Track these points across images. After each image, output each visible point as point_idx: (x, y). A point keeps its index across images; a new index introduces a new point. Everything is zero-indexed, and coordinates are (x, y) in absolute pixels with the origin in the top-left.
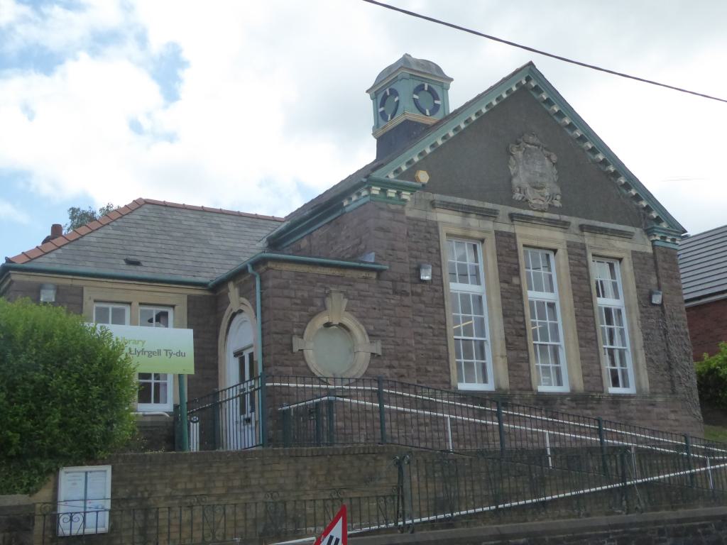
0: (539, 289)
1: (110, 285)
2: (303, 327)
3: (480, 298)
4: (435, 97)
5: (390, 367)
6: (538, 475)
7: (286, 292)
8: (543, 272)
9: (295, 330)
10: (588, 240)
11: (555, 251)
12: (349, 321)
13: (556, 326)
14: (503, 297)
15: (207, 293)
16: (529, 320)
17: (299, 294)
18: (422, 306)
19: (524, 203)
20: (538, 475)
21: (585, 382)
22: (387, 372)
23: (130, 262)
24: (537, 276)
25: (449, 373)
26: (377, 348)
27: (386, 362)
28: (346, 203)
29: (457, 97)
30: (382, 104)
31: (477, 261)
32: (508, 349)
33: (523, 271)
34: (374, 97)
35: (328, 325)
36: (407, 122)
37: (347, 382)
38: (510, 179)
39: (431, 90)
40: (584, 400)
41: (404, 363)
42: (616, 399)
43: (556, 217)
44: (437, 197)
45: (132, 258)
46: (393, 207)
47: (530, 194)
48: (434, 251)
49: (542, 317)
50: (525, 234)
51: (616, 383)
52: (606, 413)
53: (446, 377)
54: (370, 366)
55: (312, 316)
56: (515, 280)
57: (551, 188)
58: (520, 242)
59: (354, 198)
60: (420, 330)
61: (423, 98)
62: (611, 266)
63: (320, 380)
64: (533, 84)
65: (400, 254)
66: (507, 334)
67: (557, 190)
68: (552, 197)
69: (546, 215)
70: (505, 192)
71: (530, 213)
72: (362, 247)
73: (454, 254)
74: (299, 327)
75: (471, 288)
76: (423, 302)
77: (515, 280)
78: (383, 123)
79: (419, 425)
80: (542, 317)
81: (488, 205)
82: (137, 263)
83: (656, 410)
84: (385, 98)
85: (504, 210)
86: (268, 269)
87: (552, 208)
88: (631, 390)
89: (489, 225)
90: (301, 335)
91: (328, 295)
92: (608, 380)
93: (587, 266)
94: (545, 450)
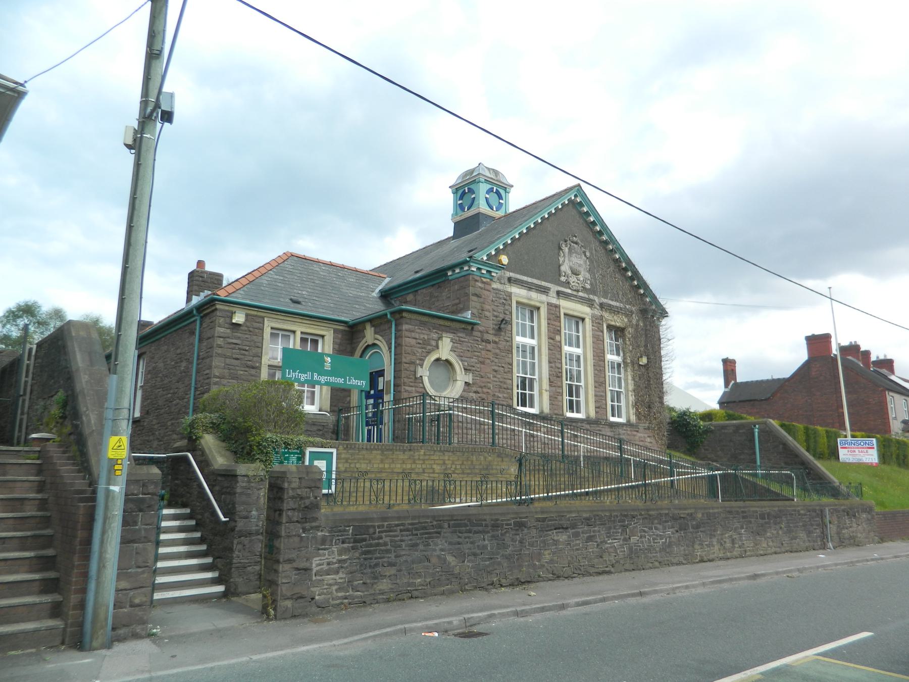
0: (524, 335)
1: (255, 313)
4: (500, 197)
5: (476, 392)
6: (324, 460)
7: (413, 335)
8: (528, 323)
9: (418, 362)
10: (606, 315)
13: (534, 364)
14: (549, 349)
15: (347, 329)
17: (422, 336)
18: (498, 351)
19: (567, 284)
20: (324, 460)
21: (596, 412)
22: (474, 396)
24: (524, 326)
26: (469, 378)
27: (474, 389)
28: (450, 273)
29: (516, 201)
30: (461, 198)
32: (550, 385)
33: (563, 331)
34: (455, 192)
35: (438, 360)
36: (478, 214)
37: (451, 400)
38: (559, 266)
39: (498, 193)
40: (595, 424)
41: (485, 390)
44: (512, 275)
46: (484, 280)
47: (573, 279)
50: (567, 306)
51: (571, 409)
53: (510, 402)
54: (464, 391)
55: (429, 353)
57: (584, 275)
58: (562, 312)
59: (457, 271)
60: (496, 368)
61: (493, 198)
62: (532, 313)
64: (579, 200)
65: (487, 314)
66: (550, 375)
67: (588, 276)
69: (581, 294)
70: (555, 275)
71: (569, 291)
74: (421, 360)
75: (528, 341)
76: (499, 349)
77: (558, 338)
78: (460, 212)
80: (524, 356)
81: (544, 284)
83: (639, 435)
84: (464, 193)
85: (554, 288)
86: (402, 317)
87: (584, 289)
88: (622, 420)
89: (543, 297)
90: (422, 366)
91: (440, 338)
92: (566, 405)
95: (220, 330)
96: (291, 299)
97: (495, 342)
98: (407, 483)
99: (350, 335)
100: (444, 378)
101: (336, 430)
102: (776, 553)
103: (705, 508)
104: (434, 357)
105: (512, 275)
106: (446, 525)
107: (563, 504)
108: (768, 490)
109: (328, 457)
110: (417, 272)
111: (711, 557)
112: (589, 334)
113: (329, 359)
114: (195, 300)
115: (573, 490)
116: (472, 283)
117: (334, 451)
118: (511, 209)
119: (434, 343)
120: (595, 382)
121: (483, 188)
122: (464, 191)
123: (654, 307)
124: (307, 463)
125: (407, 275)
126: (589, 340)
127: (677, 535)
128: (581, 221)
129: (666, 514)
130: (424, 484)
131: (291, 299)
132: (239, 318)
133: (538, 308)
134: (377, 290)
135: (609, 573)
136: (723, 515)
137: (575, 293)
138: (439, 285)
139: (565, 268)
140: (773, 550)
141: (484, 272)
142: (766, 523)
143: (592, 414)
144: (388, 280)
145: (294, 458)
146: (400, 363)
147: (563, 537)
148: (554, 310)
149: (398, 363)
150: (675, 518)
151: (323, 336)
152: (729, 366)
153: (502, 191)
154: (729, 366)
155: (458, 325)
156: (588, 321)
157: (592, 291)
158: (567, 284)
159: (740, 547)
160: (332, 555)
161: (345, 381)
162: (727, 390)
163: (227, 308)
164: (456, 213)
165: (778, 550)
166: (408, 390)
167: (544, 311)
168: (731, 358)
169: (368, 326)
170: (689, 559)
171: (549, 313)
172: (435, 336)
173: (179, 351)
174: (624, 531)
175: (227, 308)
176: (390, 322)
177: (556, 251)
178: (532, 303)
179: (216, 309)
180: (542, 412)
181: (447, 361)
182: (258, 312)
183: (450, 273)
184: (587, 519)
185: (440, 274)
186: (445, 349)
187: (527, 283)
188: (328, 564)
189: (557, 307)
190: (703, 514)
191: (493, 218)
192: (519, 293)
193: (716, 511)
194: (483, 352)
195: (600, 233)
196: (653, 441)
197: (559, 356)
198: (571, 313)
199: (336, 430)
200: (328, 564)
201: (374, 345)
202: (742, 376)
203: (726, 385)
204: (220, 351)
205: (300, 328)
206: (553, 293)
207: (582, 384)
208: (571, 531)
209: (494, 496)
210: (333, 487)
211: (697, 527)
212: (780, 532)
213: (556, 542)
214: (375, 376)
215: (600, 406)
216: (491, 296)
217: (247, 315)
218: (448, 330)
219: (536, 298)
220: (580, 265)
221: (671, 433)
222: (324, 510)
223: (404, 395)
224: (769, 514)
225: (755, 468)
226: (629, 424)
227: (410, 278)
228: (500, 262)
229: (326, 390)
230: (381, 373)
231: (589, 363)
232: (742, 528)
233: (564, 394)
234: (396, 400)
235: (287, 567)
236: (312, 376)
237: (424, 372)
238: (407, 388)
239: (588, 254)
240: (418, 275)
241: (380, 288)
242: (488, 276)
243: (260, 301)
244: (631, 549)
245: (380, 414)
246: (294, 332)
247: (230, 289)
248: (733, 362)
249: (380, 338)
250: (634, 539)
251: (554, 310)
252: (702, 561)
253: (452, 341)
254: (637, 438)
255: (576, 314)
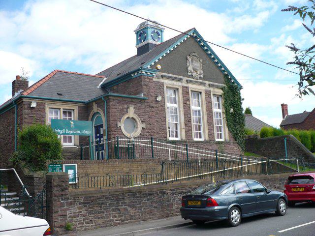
2: (120, 119)
3: (176, 108)
10: (211, 89)
11: (201, 93)
12: (135, 117)
13: (177, 116)
16: (192, 116)
19: (192, 76)
23: (59, 94)
25: (166, 134)
26: (144, 126)
28: (132, 75)
29: (167, 36)
31: (175, 96)
34: (137, 33)
35: (128, 118)
38: (187, 68)
39: (157, 33)
40: (210, 142)
41: (152, 131)
42: (219, 143)
43: (201, 81)
44: (163, 74)
45: (59, 93)
46: (149, 78)
47: (194, 74)
48: (162, 92)
49: (217, 117)
52: (215, 147)
55: (123, 115)
56: (188, 103)
57: (200, 71)
59: (136, 74)
63: (128, 138)
64: (195, 35)
67: (202, 72)
68: (200, 74)
69: (198, 80)
70: (185, 72)
71: (192, 79)
72: (138, 91)
73: (169, 94)
74: (119, 119)
77: (188, 103)
79: (157, 151)
80: (217, 117)
81: (180, 77)
82: (61, 95)
84: (141, 34)
85: (185, 79)
86: (109, 99)
87: (200, 78)
88: (223, 140)
89: (180, 84)
90: (120, 122)
91: (128, 108)
93: (211, 98)
94: (198, 160)
95: (25, 111)
96: (58, 94)
97: (156, 107)
98: (108, 177)
99: (86, 110)
100: (130, 129)
101: (81, 154)
105: (163, 74)
106: (127, 195)
107: (184, 182)
108: (285, 167)
109: (73, 168)
110: (118, 75)
112: (204, 99)
113: (73, 123)
114: (16, 94)
115: (189, 176)
116: (143, 79)
117: (76, 165)
118: (164, 40)
119: (125, 110)
120: (208, 123)
121: (150, 31)
122: (141, 33)
123: (236, 84)
124: (64, 171)
125: (114, 76)
126: (204, 102)
128: (197, 45)
130: (119, 177)
131: (58, 94)
132: (34, 105)
133: (178, 89)
134: (100, 85)
137: (195, 80)
138: (128, 81)
139: (190, 68)
141: (149, 74)
143: (207, 138)
144: (105, 79)
145: (58, 169)
146: (109, 121)
148: (186, 91)
149: (108, 121)
151: (73, 110)
152: (284, 107)
153: (159, 32)
154: (284, 107)
155: (137, 101)
156: (203, 93)
157: (204, 79)
158: (192, 76)
160: (75, 209)
161: (81, 132)
162: (284, 119)
163: (28, 100)
164: (138, 44)
166: (114, 133)
167: (180, 90)
168: (285, 103)
169: (94, 104)
171: (183, 91)
172: (126, 106)
173: (9, 121)
175: (28, 100)
176: (103, 101)
177: (185, 60)
178: (175, 87)
179: (23, 101)
180: (182, 139)
181: (133, 118)
182: (42, 102)
183: (132, 75)
185: (129, 75)
186: (131, 112)
187: (171, 77)
188: (74, 213)
189: (187, 88)
191: (156, 46)
192: (167, 82)
194: (151, 113)
197: (189, 112)
198: (193, 90)
199: (81, 154)
200: (74, 213)
201: (98, 113)
202: (291, 112)
203: (284, 117)
204: (26, 120)
205: (62, 107)
206: (184, 81)
207: (202, 124)
209: (153, 181)
210: (77, 181)
214: (98, 128)
215: (211, 134)
216: (153, 85)
217: (37, 103)
218: (132, 103)
219: (176, 84)
220: (197, 67)
221: (246, 143)
222: (70, 190)
223: (113, 136)
225: (286, 158)
226: (225, 142)
227: (117, 78)
228: (157, 68)
229: (77, 137)
230: (101, 126)
231: (204, 114)
233: (193, 130)
234: (109, 139)
235: (56, 214)
236: (66, 131)
237: (122, 125)
238: (113, 133)
239: (201, 61)
240: (119, 76)
241: (101, 83)
242: (151, 75)
243: (43, 96)
245: (103, 147)
246: (60, 109)
247: (32, 89)
248: (286, 106)
249: (100, 109)
251: (186, 91)
253: (134, 108)
254: (230, 148)
255: (196, 90)
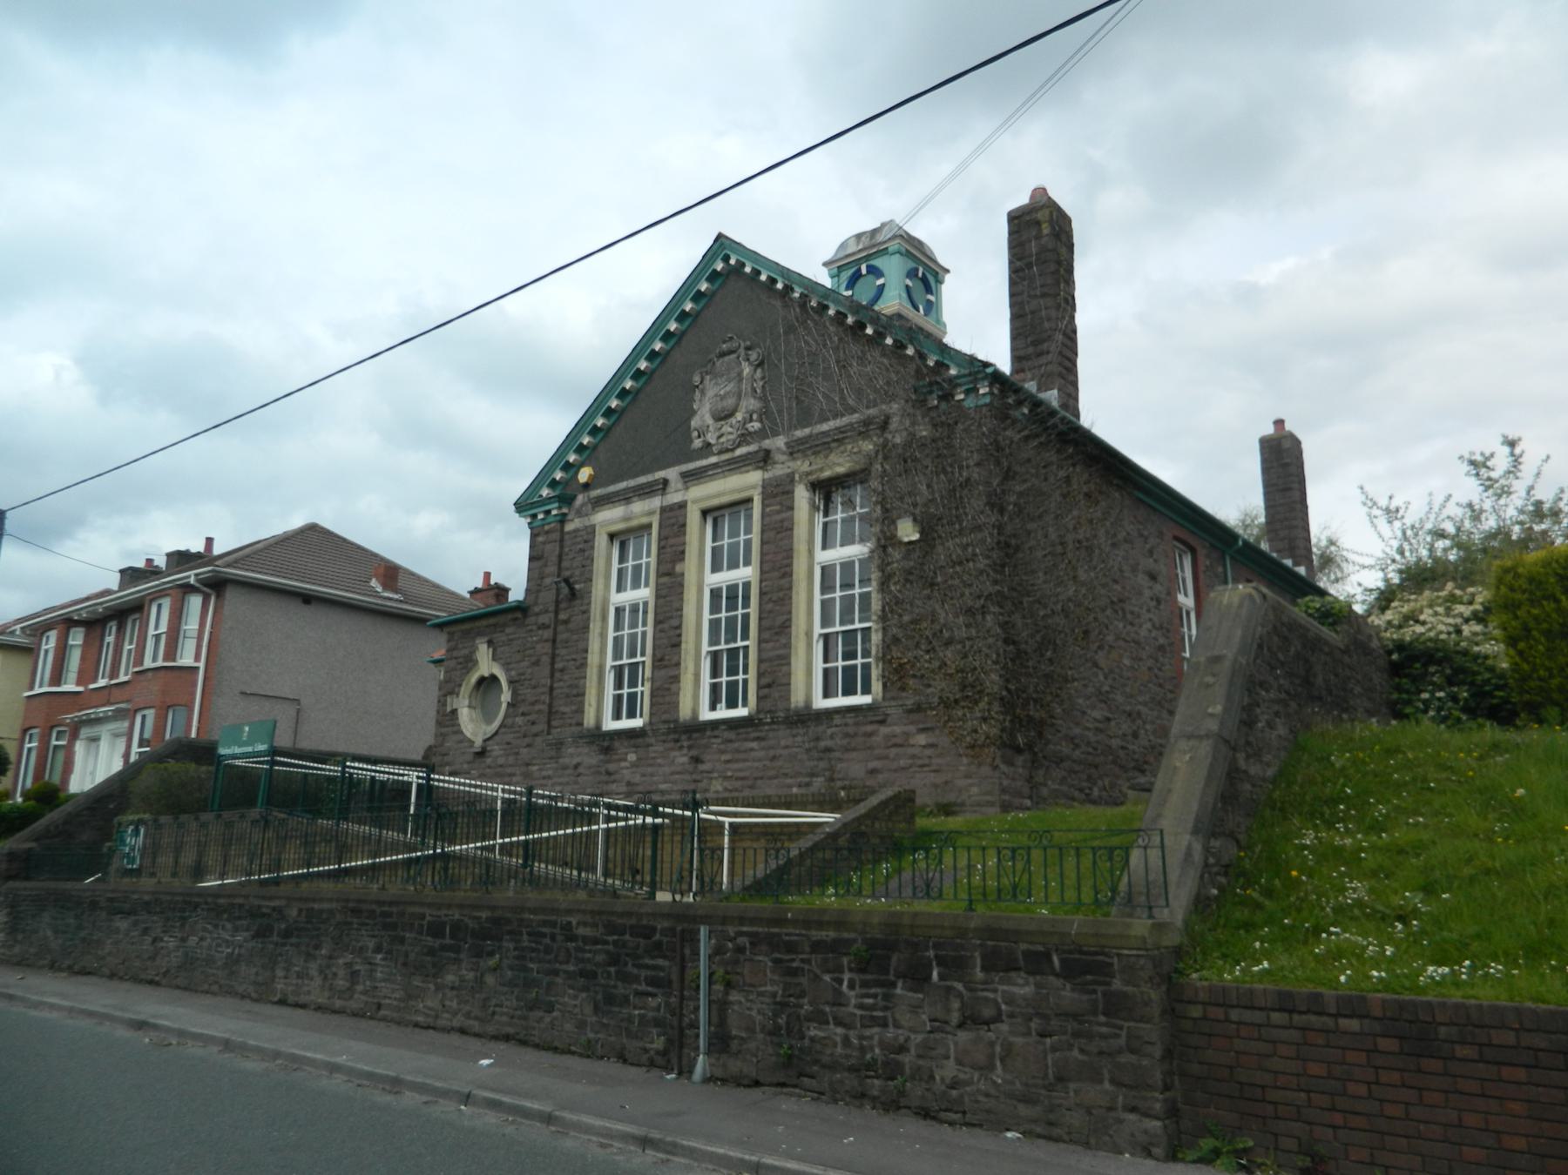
83: (884, 730)
102: (463, 1031)
103: (306, 900)
104: (474, 678)
111: (303, 999)
127: (250, 945)
129: (241, 906)
135: (157, 984)
136: (339, 918)
140: (457, 1022)
142: (443, 948)
147: (122, 924)
150: (255, 914)
159: (365, 993)
165: (475, 1026)
170: (262, 994)
174: (183, 926)
178: (635, 523)
184: (147, 903)
187: (617, 493)
190: (300, 910)
193: (326, 906)
195: (788, 289)
196: (945, 741)
208: (133, 918)
211: (287, 934)
212: (490, 980)
213: (117, 931)
224: (457, 928)
232: (378, 949)
244: (186, 954)
250: (193, 940)
252: (282, 1002)
254: (878, 739)
